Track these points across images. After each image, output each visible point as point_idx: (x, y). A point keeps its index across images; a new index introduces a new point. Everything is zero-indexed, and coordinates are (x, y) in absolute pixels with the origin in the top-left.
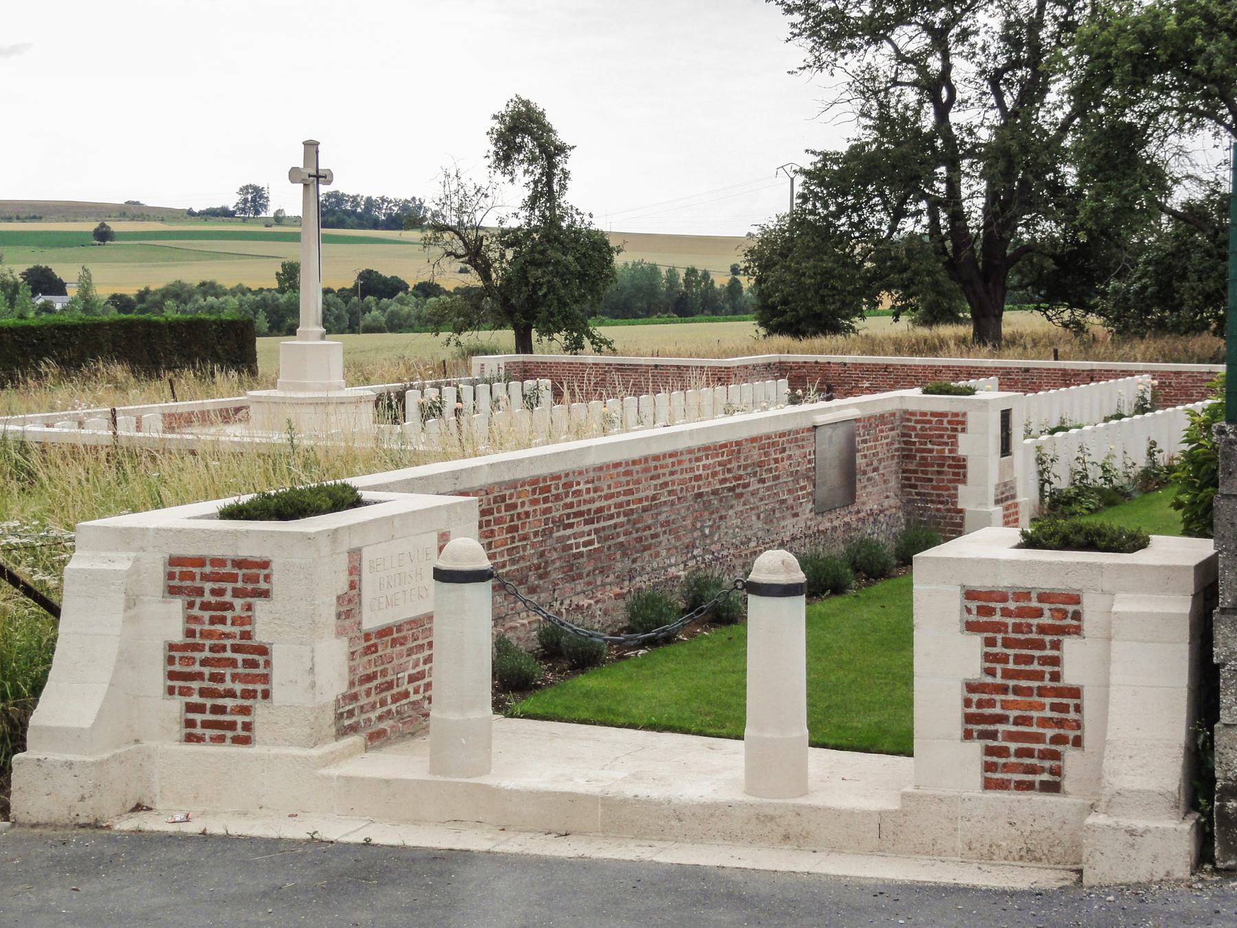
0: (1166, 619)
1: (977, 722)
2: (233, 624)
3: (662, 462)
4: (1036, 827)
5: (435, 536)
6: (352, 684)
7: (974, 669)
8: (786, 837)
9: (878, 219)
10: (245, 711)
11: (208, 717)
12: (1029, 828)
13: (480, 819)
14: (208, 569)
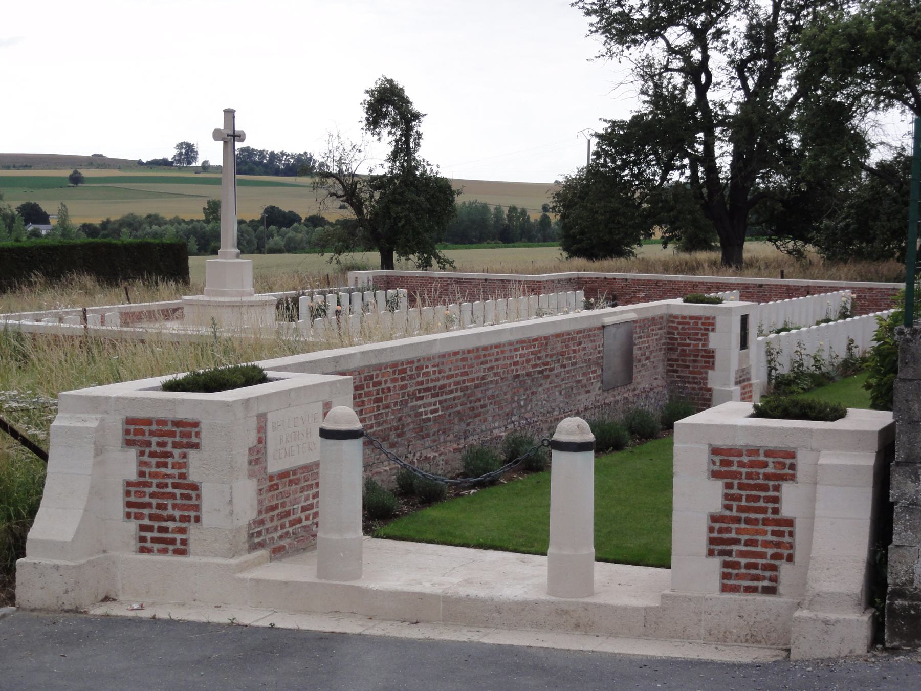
1: (718, 544)
2: (173, 468)
3: (489, 351)
4: (758, 619)
5: (321, 405)
6: (260, 512)
7: (716, 505)
8: (577, 626)
9: (653, 172)
10: (182, 531)
11: (156, 535)
12: (753, 620)
13: (354, 611)
14: (154, 427)
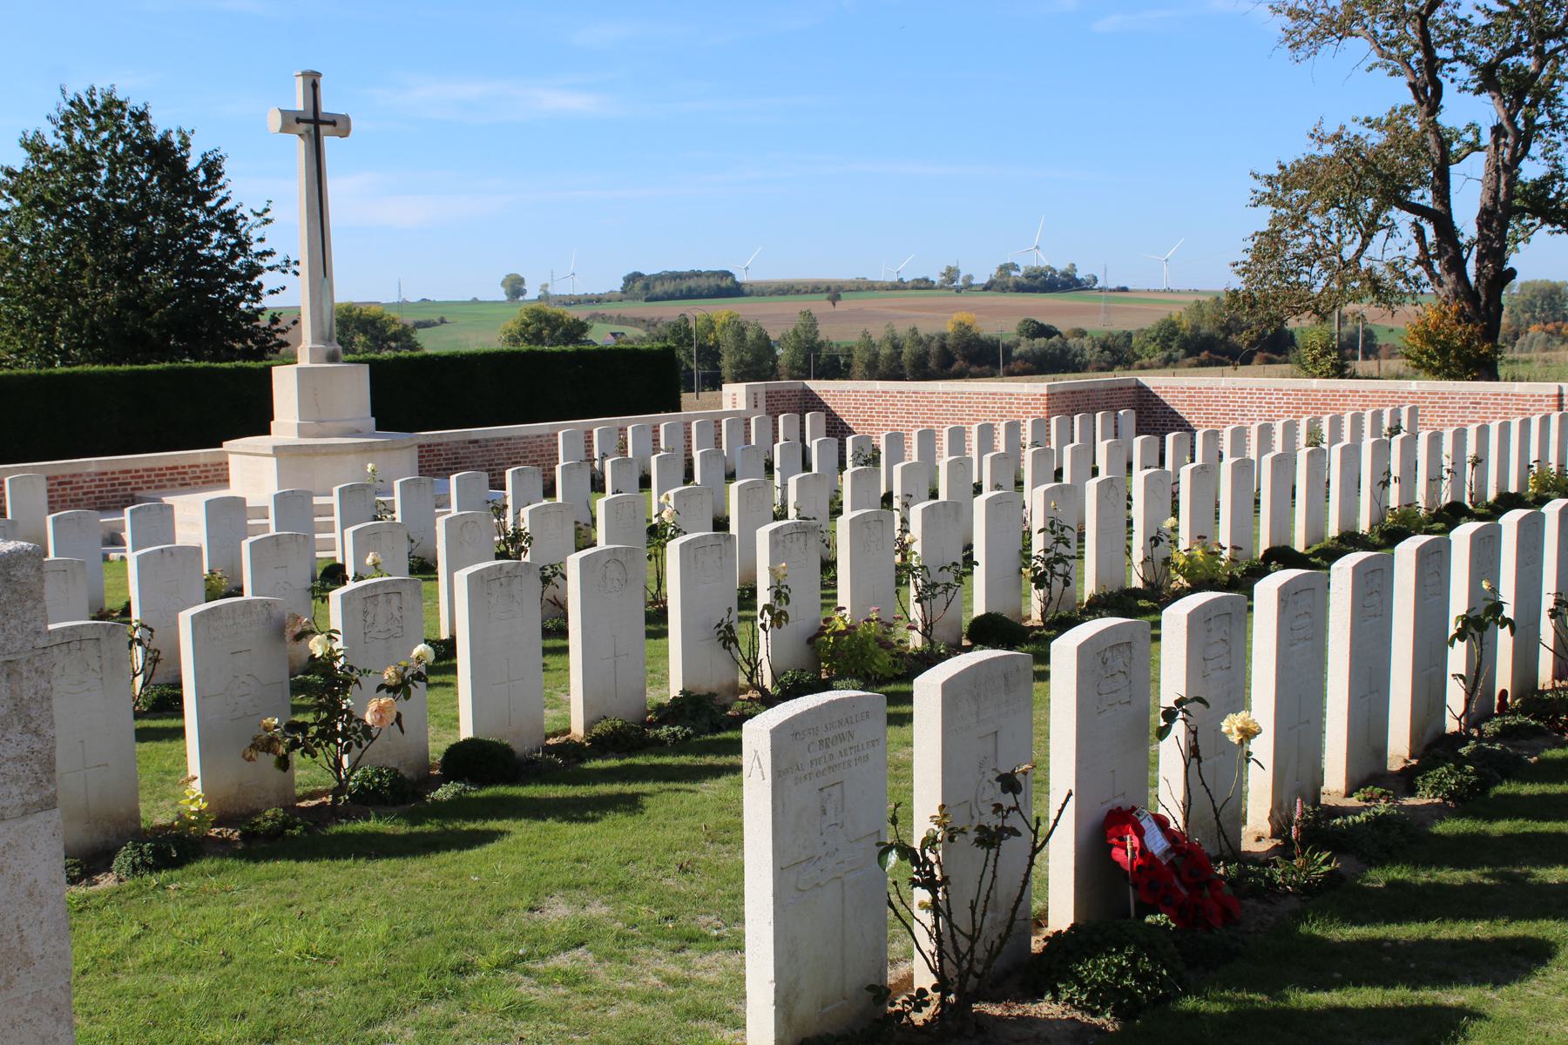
0: (1356, 525)
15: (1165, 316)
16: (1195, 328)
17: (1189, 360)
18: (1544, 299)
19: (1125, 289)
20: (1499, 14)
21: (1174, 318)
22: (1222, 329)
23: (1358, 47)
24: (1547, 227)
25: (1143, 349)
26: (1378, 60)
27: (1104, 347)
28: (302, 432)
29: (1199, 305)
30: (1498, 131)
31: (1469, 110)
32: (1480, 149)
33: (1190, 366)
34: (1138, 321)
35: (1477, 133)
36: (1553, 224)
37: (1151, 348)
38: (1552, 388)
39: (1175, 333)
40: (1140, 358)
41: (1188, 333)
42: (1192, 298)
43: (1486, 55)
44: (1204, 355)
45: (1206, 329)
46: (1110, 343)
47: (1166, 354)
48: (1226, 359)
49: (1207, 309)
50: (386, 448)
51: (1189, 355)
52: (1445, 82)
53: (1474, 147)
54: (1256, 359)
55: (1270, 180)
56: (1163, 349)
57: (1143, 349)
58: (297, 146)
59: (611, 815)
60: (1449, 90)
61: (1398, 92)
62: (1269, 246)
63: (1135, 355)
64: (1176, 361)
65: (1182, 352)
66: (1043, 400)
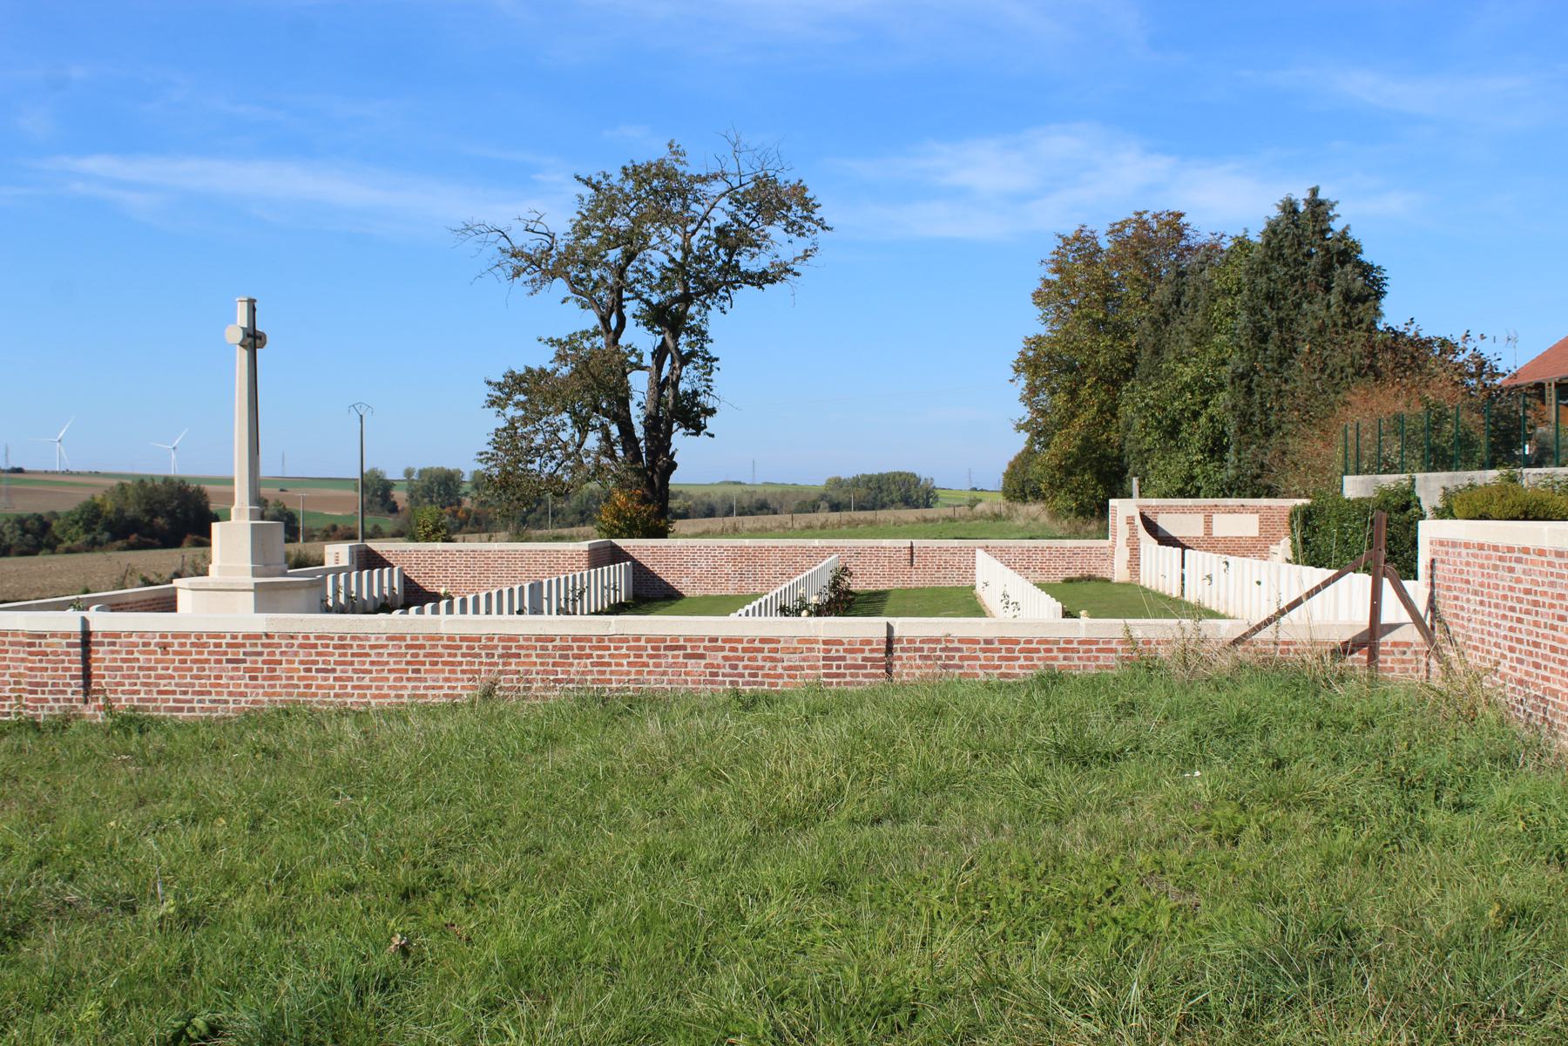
15: (87, 498)
16: (120, 511)
17: (119, 543)
18: (440, 484)
19: (20, 471)
20: (671, 270)
21: (98, 501)
22: (147, 512)
23: (560, 286)
24: (683, 430)
25: (65, 531)
26: (570, 294)
27: (25, 531)
28: (255, 574)
29: (123, 486)
30: (660, 354)
31: (640, 339)
32: (643, 369)
33: (119, 549)
34: (65, 504)
35: (640, 356)
36: (687, 427)
37: (73, 530)
38: (907, 543)
39: (98, 516)
40: (61, 541)
41: (112, 516)
42: (115, 482)
43: (655, 299)
44: (134, 538)
45: (132, 511)
46: (28, 525)
47: (89, 537)
48: (156, 541)
49: (130, 492)
50: (1115, 536)
51: (114, 538)
52: (627, 312)
53: (639, 367)
54: (186, 541)
55: (499, 386)
56: (87, 532)
57: (65, 531)
58: (242, 356)
59: (1347, 636)
60: (630, 322)
61: (591, 320)
62: (508, 439)
63: (56, 538)
64: (101, 544)
65: (107, 535)
66: (585, 555)
